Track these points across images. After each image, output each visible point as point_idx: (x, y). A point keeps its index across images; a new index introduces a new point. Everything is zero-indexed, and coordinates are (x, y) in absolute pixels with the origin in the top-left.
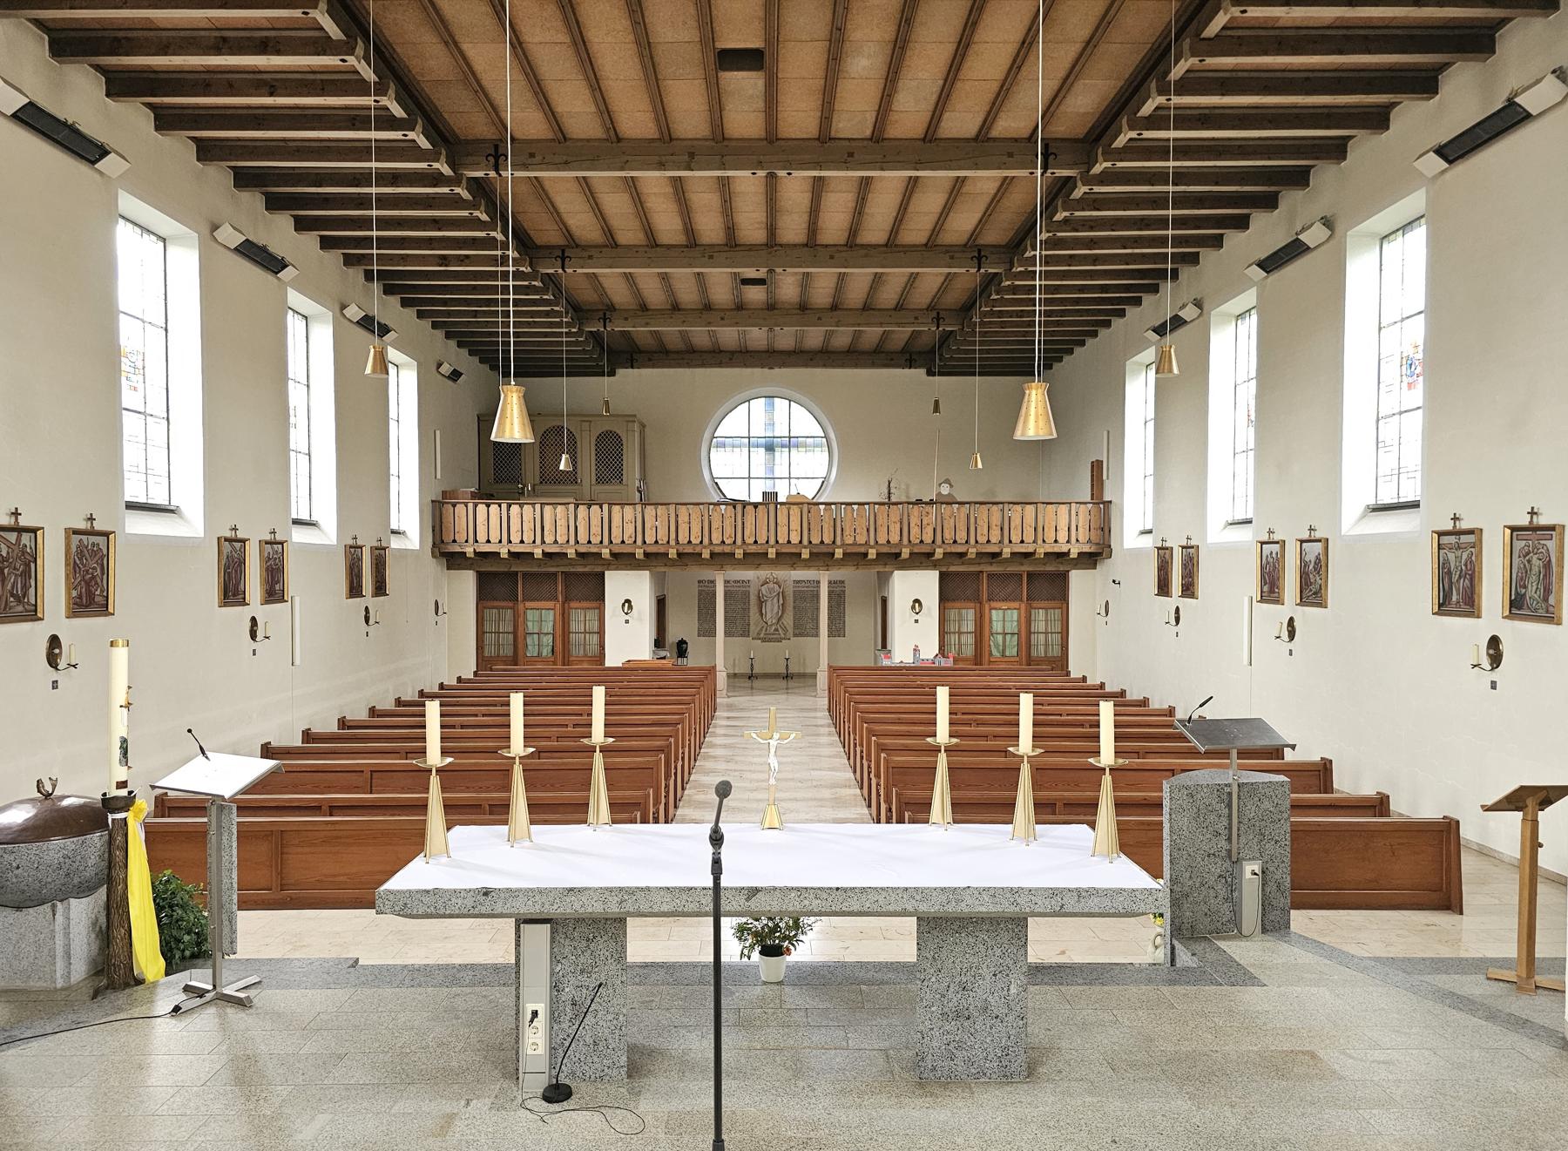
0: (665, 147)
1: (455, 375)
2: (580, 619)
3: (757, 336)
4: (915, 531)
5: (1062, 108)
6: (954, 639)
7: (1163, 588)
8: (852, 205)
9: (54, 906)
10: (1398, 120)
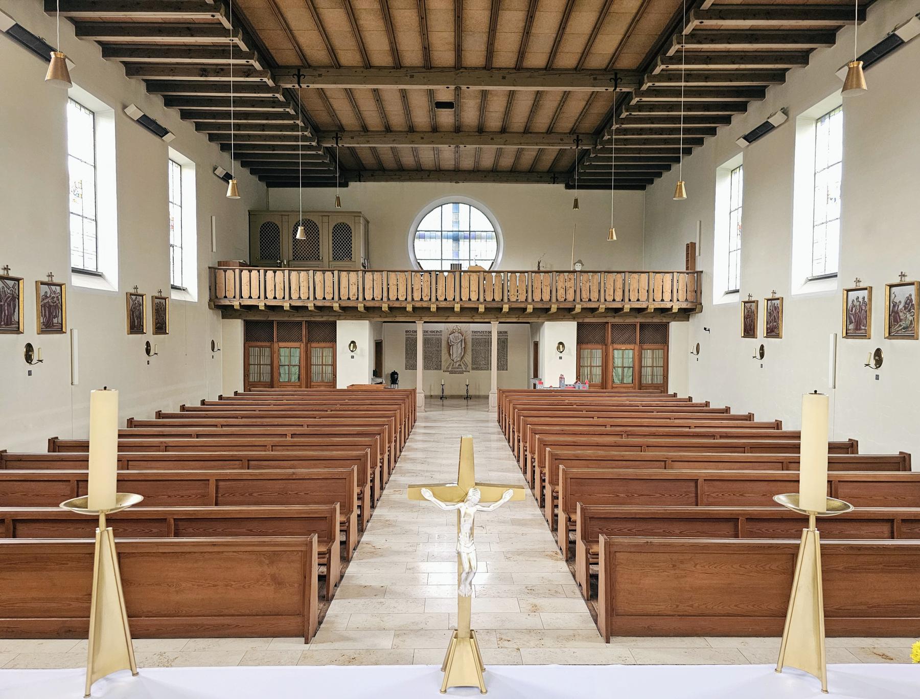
2: (319, 354)
3: (447, 154)
4: (561, 292)
6: (586, 371)
8: (521, 24)
10: (841, 37)
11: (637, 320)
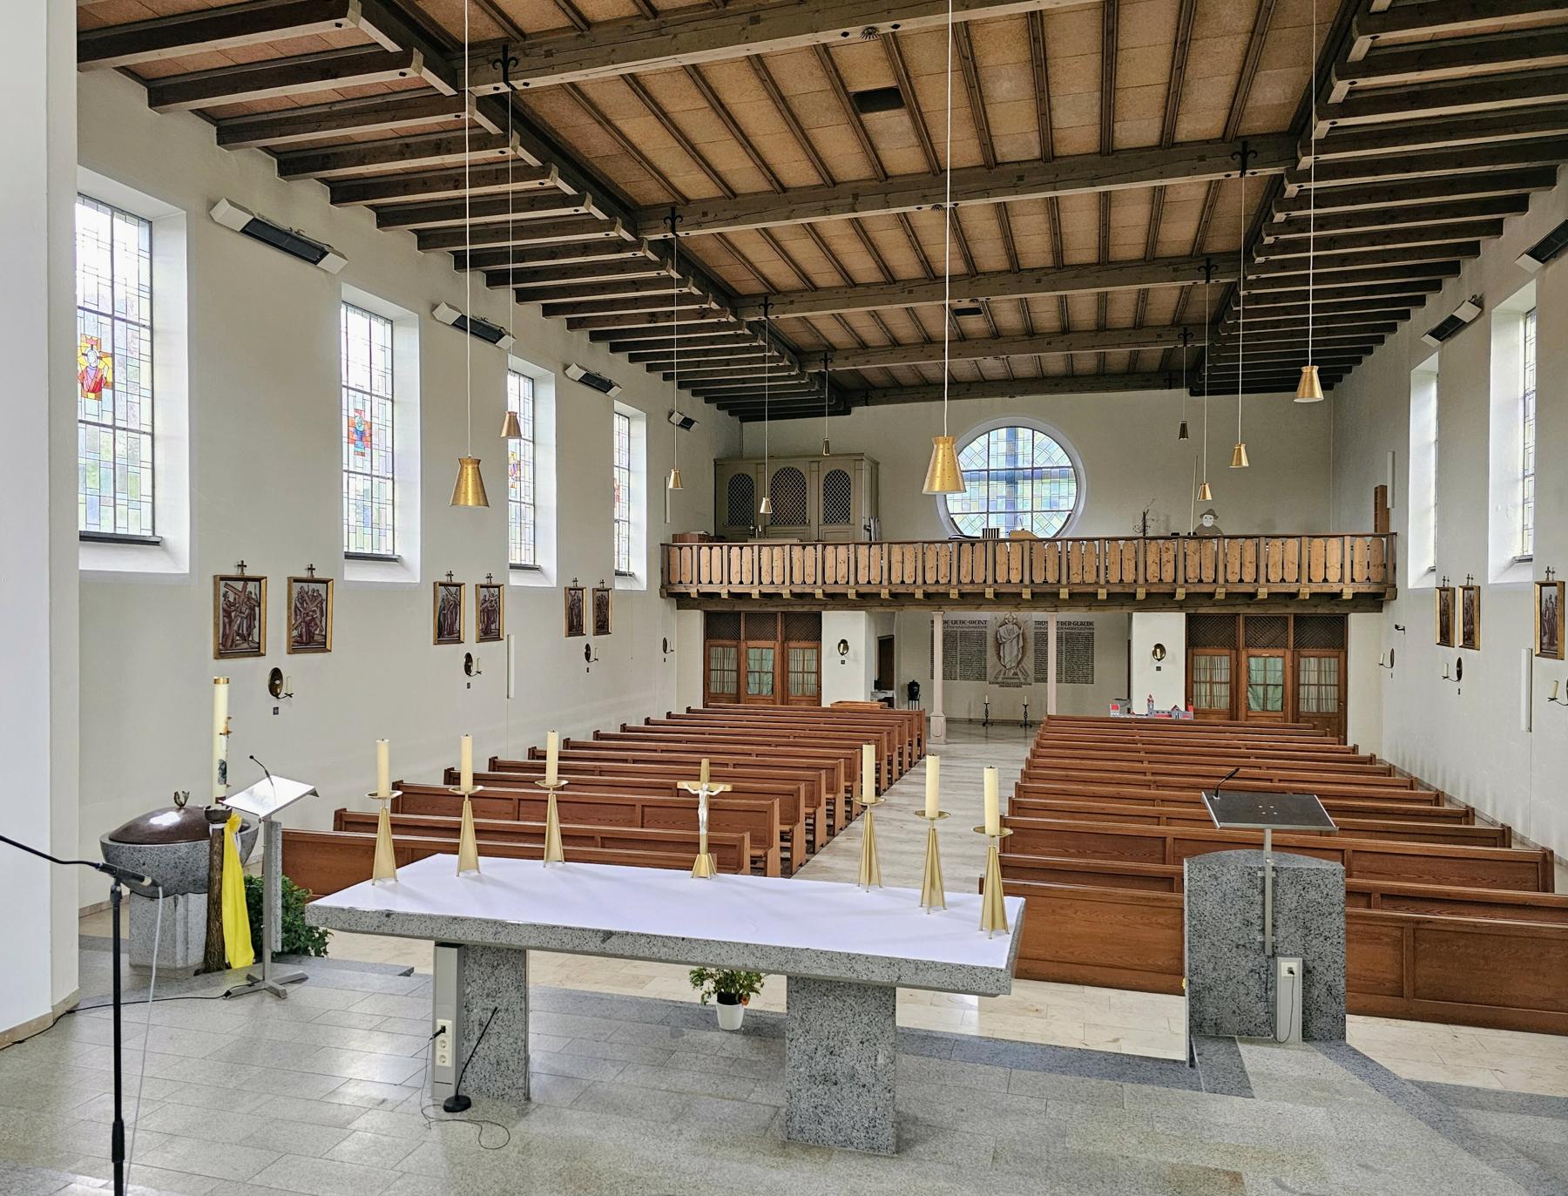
0: (831, 191)
1: (687, 423)
2: (799, 657)
5: (1250, 104)
6: (1204, 689)
7: (1446, 638)
8: (1045, 226)
9: (176, 900)
11: (1289, 610)
